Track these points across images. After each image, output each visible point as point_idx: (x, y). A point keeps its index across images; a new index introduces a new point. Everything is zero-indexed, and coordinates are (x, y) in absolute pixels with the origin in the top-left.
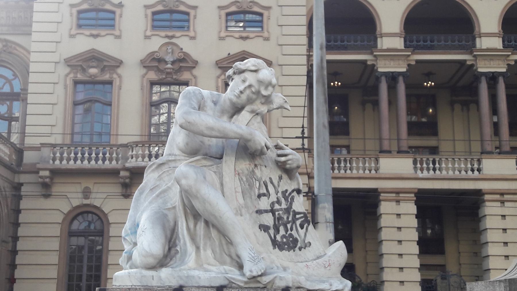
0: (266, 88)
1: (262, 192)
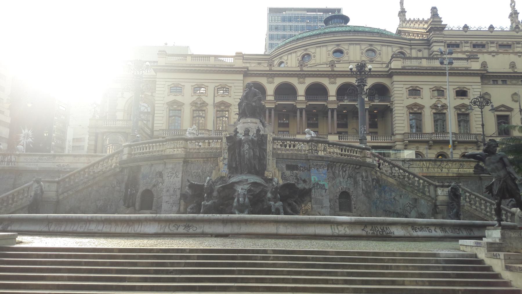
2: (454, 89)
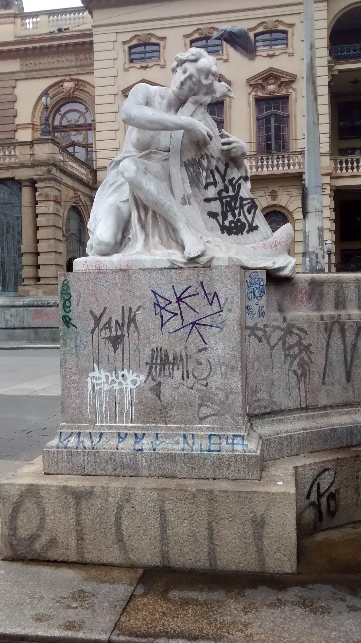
0: (207, 77)
1: (209, 181)
2: (186, 36)
